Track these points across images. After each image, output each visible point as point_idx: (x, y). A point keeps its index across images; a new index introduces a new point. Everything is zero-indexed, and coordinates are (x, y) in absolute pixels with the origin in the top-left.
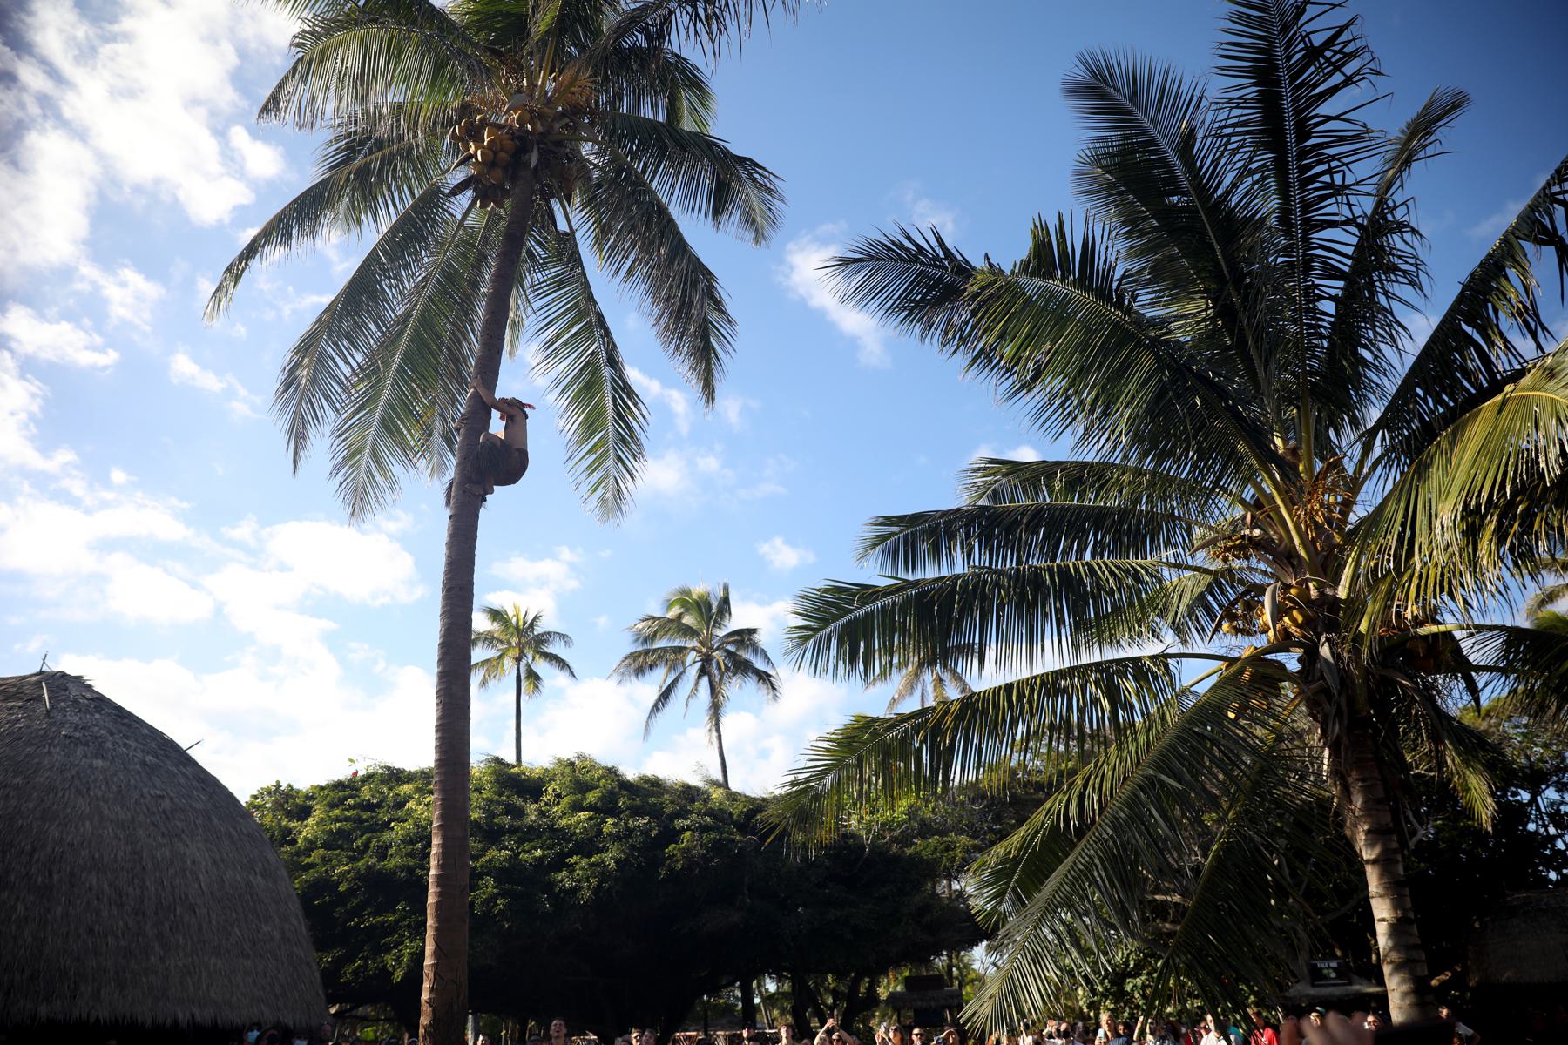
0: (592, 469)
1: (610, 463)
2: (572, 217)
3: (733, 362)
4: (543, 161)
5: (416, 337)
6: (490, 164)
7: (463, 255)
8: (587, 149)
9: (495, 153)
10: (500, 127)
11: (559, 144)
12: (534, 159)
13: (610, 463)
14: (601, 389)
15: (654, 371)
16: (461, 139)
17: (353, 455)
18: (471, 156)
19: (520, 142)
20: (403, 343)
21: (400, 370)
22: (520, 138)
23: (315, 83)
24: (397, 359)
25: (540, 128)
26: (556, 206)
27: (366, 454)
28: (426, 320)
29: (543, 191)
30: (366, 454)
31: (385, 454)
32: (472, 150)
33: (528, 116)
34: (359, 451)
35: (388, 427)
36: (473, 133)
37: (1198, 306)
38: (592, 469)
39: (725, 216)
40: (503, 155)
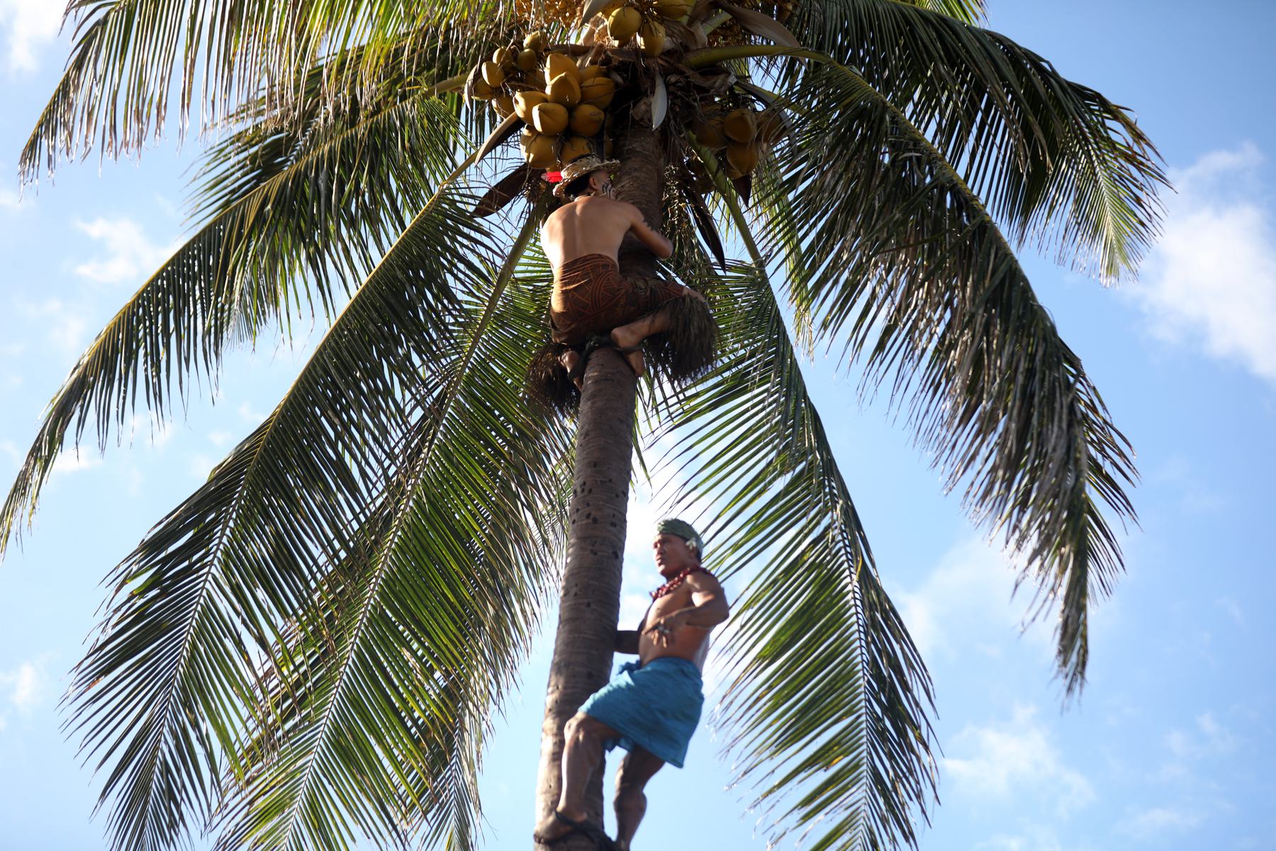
0: (813, 804)
1: (859, 793)
2: (741, 233)
3: (1131, 540)
4: (681, 110)
5: (416, 545)
6: (561, 136)
7: (516, 343)
8: (765, 77)
9: (571, 109)
10: (576, 52)
11: (712, 69)
12: (658, 108)
13: (859, 793)
14: (838, 620)
15: (954, 569)
16: (496, 92)
17: (265, 815)
18: (517, 124)
19: (626, 76)
20: (383, 564)
21: (378, 619)
22: (622, 68)
23: (144, 51)
24: (371, 595)
25: (664, 40)
26: (718, 210)
27: (296, 812)
28: (435, 509)
29: (684, 182)
30: (296, 812)
31: (337, 813)
32: (520, 110)
33: (634, 16)
34: (278, 807)
35: (349, 753)
36: (520, 72)
37: (609, 756)
38: (813, 804)
39: (1040, 213)
40: (587, 110)
